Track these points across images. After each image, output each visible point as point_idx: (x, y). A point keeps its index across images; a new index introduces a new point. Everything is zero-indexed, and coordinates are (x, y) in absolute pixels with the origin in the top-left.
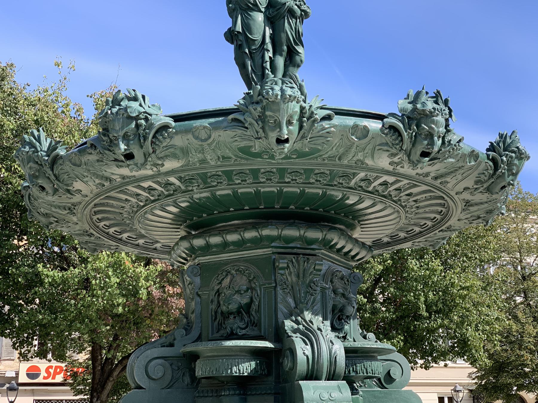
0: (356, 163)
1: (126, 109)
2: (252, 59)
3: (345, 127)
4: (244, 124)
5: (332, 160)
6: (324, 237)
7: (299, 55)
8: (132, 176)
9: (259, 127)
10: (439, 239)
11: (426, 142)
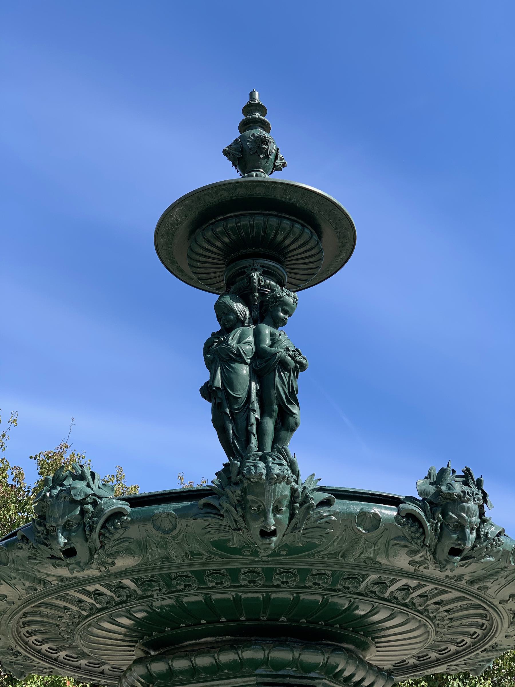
0: (365, 562)
1: (69, 490)
2: (234, 421)
3: (350, 514)
4: (219, 510)
5: (333, 558)
6: (325, 661)
7: (293, 416)
8: (72, 578)
9: (239, 515)
10: (482, 661)
11: (455, 536)
